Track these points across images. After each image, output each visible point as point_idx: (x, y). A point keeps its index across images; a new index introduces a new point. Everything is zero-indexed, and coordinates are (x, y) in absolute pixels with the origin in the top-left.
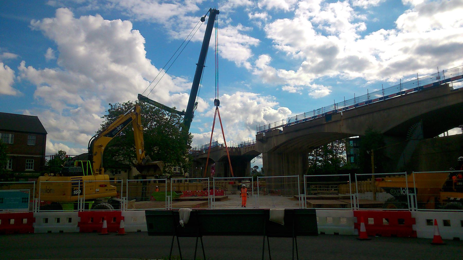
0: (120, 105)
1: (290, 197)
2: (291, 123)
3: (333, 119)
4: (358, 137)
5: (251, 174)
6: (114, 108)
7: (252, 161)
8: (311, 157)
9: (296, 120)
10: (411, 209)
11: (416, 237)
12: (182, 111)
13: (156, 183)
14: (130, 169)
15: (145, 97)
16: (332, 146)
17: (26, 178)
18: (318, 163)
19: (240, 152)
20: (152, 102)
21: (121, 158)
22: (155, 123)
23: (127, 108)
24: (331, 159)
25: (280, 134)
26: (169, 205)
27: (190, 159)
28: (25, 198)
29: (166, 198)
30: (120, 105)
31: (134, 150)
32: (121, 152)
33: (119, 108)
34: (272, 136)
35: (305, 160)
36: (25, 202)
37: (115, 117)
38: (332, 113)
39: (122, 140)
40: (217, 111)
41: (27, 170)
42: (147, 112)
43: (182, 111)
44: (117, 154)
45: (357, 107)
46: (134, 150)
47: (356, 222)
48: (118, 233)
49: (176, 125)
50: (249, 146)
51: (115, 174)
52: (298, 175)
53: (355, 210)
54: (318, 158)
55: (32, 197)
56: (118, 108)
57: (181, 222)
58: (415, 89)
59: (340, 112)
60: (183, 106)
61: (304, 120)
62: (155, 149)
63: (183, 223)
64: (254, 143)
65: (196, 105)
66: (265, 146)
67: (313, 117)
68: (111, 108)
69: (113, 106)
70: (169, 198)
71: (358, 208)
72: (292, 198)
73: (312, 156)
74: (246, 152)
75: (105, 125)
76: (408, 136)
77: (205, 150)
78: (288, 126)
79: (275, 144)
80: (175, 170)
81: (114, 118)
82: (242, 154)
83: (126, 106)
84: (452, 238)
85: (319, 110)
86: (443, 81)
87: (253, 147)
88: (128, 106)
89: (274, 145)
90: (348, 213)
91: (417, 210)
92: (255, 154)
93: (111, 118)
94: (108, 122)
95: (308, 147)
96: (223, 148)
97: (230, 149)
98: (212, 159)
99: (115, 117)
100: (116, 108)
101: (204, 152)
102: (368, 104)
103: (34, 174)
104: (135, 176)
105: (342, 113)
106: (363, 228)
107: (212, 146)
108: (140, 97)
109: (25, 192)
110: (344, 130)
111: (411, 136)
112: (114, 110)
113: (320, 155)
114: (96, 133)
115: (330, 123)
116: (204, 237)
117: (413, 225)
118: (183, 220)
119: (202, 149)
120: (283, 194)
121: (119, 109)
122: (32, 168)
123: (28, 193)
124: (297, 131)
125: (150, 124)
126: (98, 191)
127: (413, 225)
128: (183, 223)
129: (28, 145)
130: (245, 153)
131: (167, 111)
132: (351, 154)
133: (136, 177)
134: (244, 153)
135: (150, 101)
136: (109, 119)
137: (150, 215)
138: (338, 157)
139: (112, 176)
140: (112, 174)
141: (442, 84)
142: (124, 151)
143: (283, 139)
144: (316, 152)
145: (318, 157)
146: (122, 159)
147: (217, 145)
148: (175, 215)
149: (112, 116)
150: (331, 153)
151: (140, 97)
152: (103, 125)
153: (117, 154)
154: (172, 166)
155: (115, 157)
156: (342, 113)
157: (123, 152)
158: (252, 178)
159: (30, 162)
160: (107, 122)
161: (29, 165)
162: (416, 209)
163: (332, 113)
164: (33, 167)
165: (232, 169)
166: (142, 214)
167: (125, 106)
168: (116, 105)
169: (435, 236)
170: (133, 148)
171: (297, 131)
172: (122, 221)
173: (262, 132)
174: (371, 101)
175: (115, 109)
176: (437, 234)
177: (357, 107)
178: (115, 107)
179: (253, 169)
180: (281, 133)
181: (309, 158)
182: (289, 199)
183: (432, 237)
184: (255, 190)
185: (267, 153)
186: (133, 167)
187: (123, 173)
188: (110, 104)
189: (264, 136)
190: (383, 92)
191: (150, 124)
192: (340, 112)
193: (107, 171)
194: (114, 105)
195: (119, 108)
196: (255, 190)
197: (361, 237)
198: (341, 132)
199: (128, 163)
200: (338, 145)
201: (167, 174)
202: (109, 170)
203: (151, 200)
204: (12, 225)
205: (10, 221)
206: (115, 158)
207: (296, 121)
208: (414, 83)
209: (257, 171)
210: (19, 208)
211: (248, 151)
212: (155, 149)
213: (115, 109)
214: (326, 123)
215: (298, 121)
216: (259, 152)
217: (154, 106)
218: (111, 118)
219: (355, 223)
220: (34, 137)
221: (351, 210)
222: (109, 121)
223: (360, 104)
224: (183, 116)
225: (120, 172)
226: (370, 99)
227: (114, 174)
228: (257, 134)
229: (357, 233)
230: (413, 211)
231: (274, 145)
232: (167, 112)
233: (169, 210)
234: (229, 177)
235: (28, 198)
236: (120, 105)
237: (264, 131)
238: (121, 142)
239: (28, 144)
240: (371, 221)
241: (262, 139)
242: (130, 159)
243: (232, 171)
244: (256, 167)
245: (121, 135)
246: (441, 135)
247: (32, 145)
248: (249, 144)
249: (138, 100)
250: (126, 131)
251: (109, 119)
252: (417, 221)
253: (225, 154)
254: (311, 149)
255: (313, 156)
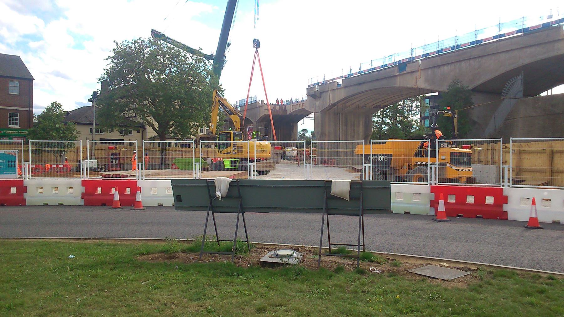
0: (128, 42)
1: (347, 169)
2: (353, 74)
3: (408, 69)
4: (436, 94)
5: (298, 139)
6: (121, 47)
7: (300, 123)
8: (375, 119)
9: (360, 69)
10: (503, 184)
11: (507, 219)
12: (210, 55)
13: (179, 147)
14: (144, 128)
15: (161, 33)
16: (404, 106)
17: (10, 137)
18: (384, 126)
19: (285, 110)
20: (170, 41)
21: (132, 114)
22: (175, 69)
23: (138, 48)
24: (401, 122)
25: (338, 87)
26: (198, 174)
27: (221, 118)
28: (12, 162)
29: (429, 168)
30: (128, 43)
31: (148, 104)
32: (132, 106)
33: (127, 47)
34: (327, 91)
35: (368, 122)
36: (12, 166)
37: (123, 59)
38: (407, 61)
39: (133, 90)
40: (257, 55)
41: (10, 126)
42: (164, 54)
43: (210, 55)
44: (127, 109)
45: (441, 54)
46: (148, 104)
47: (433, 199)
48: (133, 208)
49: (203, 73)
50: (297, 104)
51: (125, 134)
52: (81, 140)
53: (433, 185)
54: (385, 121)
55: (20, 161)
56: (125, 47)
57: (218, 194)
58: (518, 31)
59: (418, 59)
60: (211, 48)
61: (370, 70)
62: (177, 104)
63: (221, 195)
64: (304, 99)
65: (228, 46)
66: (317, 103)
67: (382, 67)
68: (117, 47)
69: (119, 44)
70: (198, 165)
71: (437, 182)
72: (349, 170)
73: (378, 118)
74: (293, 111)
75: (110, 69)
76: (504, 93)
77: (240, 107)
78: (349, 77)
79: (331, 101)
80: (202, 131)
81: (120, 61)
82: (288, 113)
83: (136, 45)
84: (550, 220)
85: (391, 57)
86: (556, 22)
87: (302, 104)
88: (139, 45)
89: (330, 102)
90: (424, 189)
91: (144, 179)
92: (303, 114)
93: (117, 60)
94: (113, 66)
95: (373, 105)
96: (263, 105)
97: (273, 106)
98: (249, 118)
99: (123, 59)
100: (123, 47)
101: (239, 110)
102: (455, 50)
103: (20, 132)
104: (151, 137)
105: (420, 61)
106: (441, 207)
107: (249, 102)
108: (154, 33)
109: (10, 154)
110: (422, 84)
111: (507, 94)
112: (121, 50)
113: (387, 116)
114: (99, 80)
115: (404, 74)
116: (247, 214)
117: (504, 205)
118: (220, 192)
119: (237, 106)
120: (339, 165)
121: (127, 48)
122: (17, 125)
123: (15, 155)
124: (360, 84)
125: (168, 69)
126: (444, 159)
127: (504, 205)
128: (220, 195)
129: (9, 94)
130: (291, 111)
131: (190, 54)
132: (426, 116)
133: (151, 139)
134: (290, 111)
135: (167, 39)
136: (115, 61)
137: (177, 185)
138: (410, 119)
139: (122, 136)
140: (121, 134)
141: (553, 26)
142: (135, 105)
143: (342, 95)
144: (382, 113)
145: (384, 119)
146: (134, 115)
147: (256, 101)
148: (210, 185)
149: (118, 58)
150: (402, 114)
151: (154, 33)
152: (107, 69)
153: (127, 109)
154: (198, 126)
155: (124, 112)
156: (420, 61)
157: (134, 105)
158: (22, 142)
159: (13, 116)
160: (112, 66)
161: (13, 120)
162: (510, 184)
163: (407, 62)
164: (18, 123)
165: (274, 132)
166: (168, 184)
167: (135, 45)
168: (124, 43)
169: (531, 218)
170: (147, 102)
171: (360, 84)
172: (138, 193)
173: (314, 84)
174: (458, 46)
175: (122, 49)
176: (534, 216)
177: (441, 54)
178: (121, 45)
179: (300, 133)
180: (340, 87)
181: (373, 120)
182: (346, 171)
183: (528, 220)
184: (308, 158)
185: (319, 113)
186: (148, 126)
187: (134, 132)
188: (114, 42)
189: (317, 90)
190: (475, 35)
191: (168, 69)
192: (418, 59)
193: (115, 130)
194: (120, 43)
195: (127, 47)
196: (308, 158)
197: (437, 218)
198: (417, 87)
199: (141, 121)
200: (410, 104)
201: (192, 136)
202: (117, 129)
203: (172, 168)
204: (13, 194)
205: (10, 189)
206: (124, 114)
207: (360, 71)
208: (517, 23)
209: (305, 136)
210: (5, 174)
211: (295, 110)
212: (177, 104)
213: (122, 49)
214: (398, 74)
215: (362, 72)
216: (310, 110)
217: (172, 46)
218: (117, 60)
219: (431, 201)
220: (17, 84)
221: (427, 184)
222: (115, 65)
223: (445, 49)
224: (212, 61)
225: (131, 133)
226: (458, 44)
227: (124, 134)
228: (308, 87)
229: (433, 213)
230: (506, 187)
231: (330, 102)
232: (191, 55)
233: (434, 185)
234: (342, 142)
235: (15, 162)
236: (128, 42)
237: (318, 84)
238: (131, 93)
239: (9, 93)
240: (452, 200)
241: (314, 94)
242: (144, 115)
243: (275, 135)
244: (305, 130)
245: (130, 83)
246: (544, 94)
247: (15, 95)
248: (297, 100)
249: (152, 37)
250: (137, 78)
251: (115, 61)
252: (509, 199)
253: (266, 113)
254: (377, 108)
255: (378, 117)
